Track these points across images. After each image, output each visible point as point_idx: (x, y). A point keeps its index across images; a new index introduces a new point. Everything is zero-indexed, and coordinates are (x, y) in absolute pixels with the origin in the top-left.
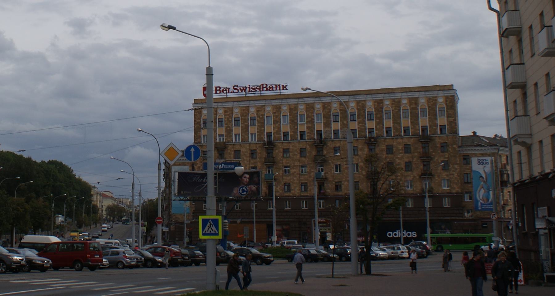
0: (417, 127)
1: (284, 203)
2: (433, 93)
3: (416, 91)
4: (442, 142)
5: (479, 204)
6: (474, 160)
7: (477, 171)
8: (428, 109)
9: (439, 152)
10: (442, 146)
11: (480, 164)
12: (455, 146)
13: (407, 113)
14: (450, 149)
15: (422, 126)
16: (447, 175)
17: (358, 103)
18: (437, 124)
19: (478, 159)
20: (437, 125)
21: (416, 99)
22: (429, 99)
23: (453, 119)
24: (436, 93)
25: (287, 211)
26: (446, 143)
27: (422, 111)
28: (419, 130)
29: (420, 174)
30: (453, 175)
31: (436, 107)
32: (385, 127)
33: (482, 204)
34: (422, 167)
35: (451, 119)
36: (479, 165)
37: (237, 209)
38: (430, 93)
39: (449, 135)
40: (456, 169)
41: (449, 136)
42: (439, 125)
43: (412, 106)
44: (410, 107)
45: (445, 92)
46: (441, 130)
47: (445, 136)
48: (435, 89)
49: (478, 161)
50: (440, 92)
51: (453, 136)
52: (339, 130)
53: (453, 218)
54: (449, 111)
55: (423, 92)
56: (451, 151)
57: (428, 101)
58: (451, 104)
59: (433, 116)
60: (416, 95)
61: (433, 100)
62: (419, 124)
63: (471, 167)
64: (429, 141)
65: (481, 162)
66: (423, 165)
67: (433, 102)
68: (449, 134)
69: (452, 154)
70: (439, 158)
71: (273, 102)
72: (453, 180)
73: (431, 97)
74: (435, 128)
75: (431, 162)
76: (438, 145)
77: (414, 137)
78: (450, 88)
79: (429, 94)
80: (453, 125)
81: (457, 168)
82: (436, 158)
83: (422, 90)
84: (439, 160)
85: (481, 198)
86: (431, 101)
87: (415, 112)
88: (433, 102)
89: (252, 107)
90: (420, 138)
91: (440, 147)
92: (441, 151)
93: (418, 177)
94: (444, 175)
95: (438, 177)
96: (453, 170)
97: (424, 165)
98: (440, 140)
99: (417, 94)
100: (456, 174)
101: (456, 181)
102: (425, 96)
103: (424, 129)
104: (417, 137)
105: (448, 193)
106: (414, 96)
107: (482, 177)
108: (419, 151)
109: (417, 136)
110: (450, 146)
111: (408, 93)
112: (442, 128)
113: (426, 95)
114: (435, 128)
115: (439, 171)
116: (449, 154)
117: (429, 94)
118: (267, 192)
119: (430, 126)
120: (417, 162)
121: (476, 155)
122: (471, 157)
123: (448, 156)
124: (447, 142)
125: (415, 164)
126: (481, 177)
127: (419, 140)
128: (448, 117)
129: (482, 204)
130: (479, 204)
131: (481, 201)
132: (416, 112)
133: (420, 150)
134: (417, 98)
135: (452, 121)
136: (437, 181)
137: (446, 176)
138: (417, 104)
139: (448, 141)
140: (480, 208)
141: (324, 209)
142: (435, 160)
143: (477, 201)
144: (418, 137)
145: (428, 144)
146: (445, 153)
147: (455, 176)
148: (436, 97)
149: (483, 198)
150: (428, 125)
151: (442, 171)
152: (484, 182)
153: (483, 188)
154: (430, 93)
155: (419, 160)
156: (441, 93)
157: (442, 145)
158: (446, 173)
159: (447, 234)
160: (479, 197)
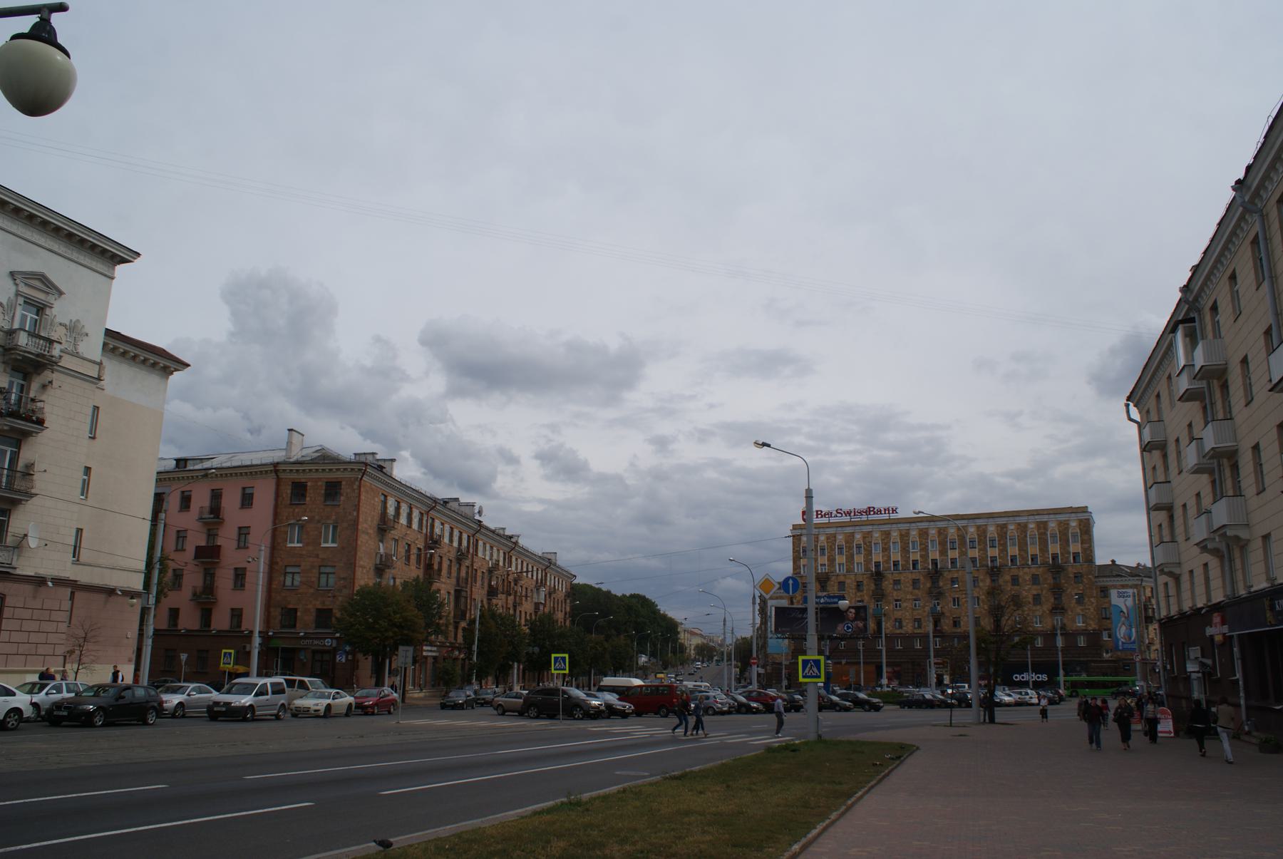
5: (1120, 643)
6: (1114, 593)
10: (1075, 577)
11: (1121, 597)
14: (1085, 580)
16: (1082, 610)
22: (1060, 523)
24: (1068, 515)
28: (1049, 558)
30: (1089, 609)
34: (1052, 600)
35: (1086, 546)
40: (1093, 603)
42: (1071, 552)
45: (1079, 515)
50: (1073, 515)
53: (1089, 659)
60: (1045, 518)
63: (1110, 601)
67: (1064, 526)
70: (1072, 591)
78: (1084, 510)
82: (1069, 590)
85: (1122, 636)
88: (1064, 526)
94: (1079, 609)
95: (1072, 611)
97: (1055, 599)
99: (1047, 517)
101: (1092, 617)
103: (1055, 557)
112: (1076, 556)
115: (1072, 605)
124: (1081, 571)
126: (1122, 611)
128: (1082, 543)
129: (1123, 643)
130: (1120, 643)
131: (1123, 640)
133: (1051, 581)
134: (1046, 522)
136: (1070, 617)
148: (1068, 520)
150: (1059, 552)
151: (1076, 605)
152: (1125, 618)
153: (1124, 624)
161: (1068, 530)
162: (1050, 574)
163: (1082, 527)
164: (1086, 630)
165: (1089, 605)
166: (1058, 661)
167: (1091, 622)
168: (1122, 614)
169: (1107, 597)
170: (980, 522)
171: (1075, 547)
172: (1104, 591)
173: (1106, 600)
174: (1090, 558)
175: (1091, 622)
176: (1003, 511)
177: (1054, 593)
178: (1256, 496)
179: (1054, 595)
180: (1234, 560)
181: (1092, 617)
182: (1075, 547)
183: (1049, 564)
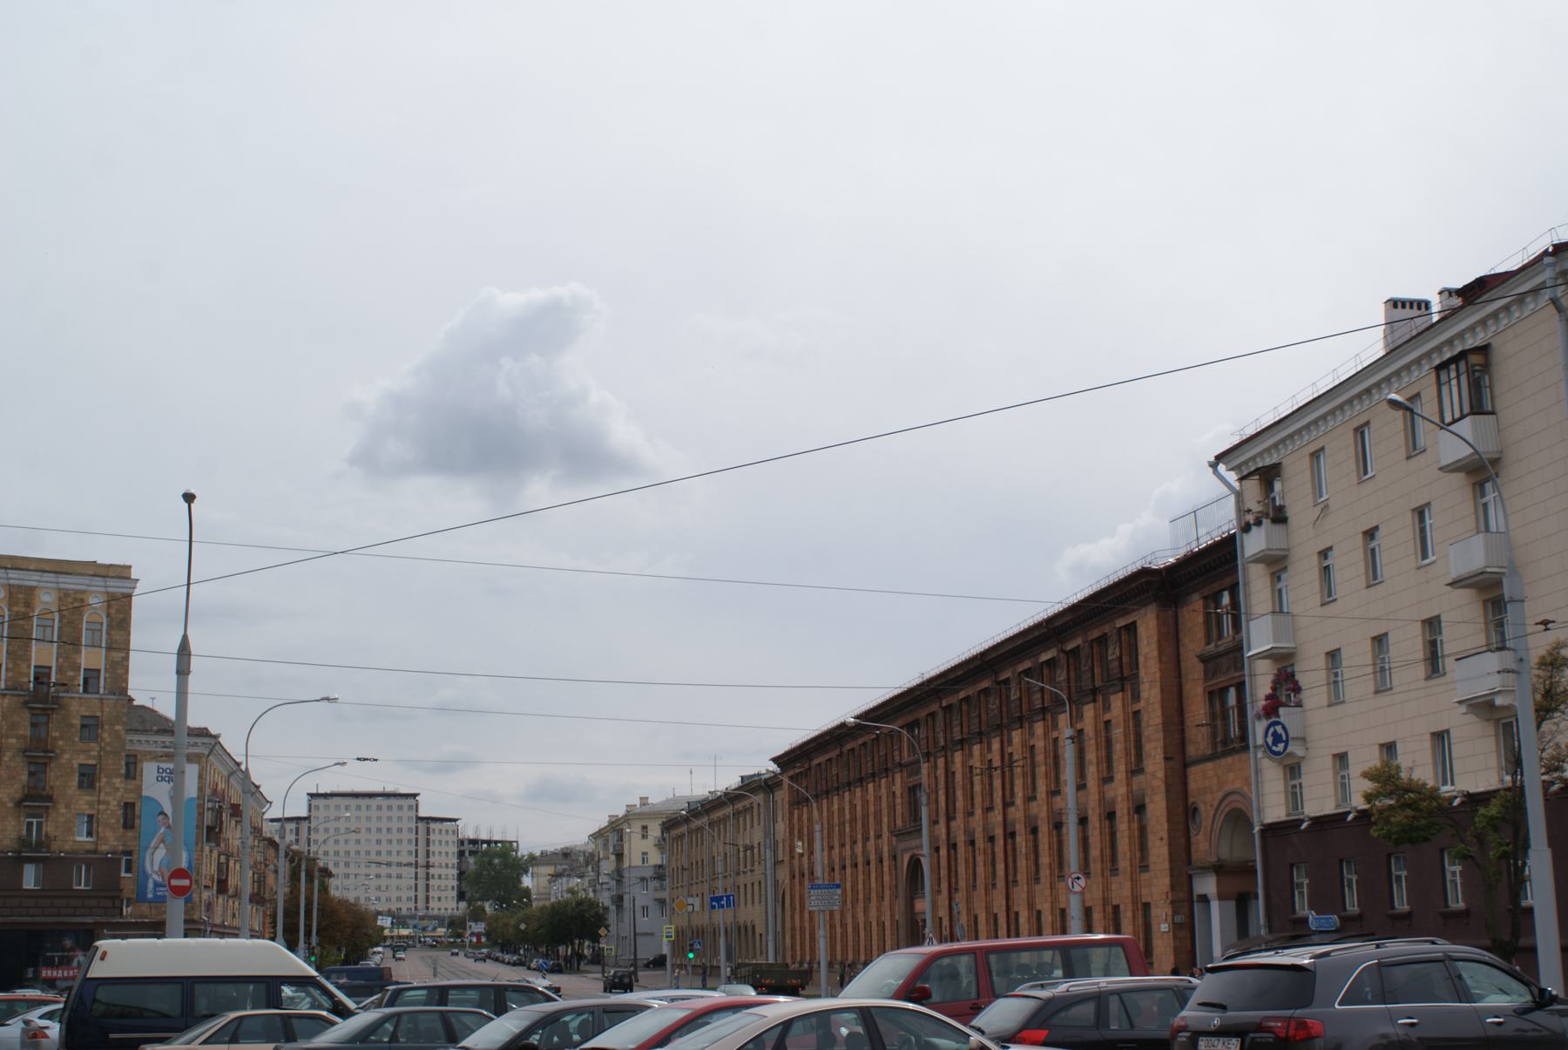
0: (24, 666)
1: (73, 869)
2: (77, 581)
3: (31, 568)
4: (87, 714)
5: (151, 885)
6: (149, 770)
7: (153, 799)
8: (60, 621)
9: (77, 739)
10: (83, 726)
11: (163, 779)
12: (117, 727)
13: (96, 632)
14: (105, 735)
15: (35, 667)
16: (91, 804)
17: (64, 595)
18: (80, 664)
19: (158, 769)
20: (80, 667)
21: (30, 591)
22: (64, 595)
23: (123, 655)
24: (86, 580)
25: (81, 895)
26: (98, 717)
27: (91, 629)
28: (28, 675)
29: (18, 796)
30: (107, 803)
31: (82, 620)
32: (33, 664)
33: (156, 885)
34: (25, 777)
35: (117, 656)
36: (160, 783)
37: (78, 888)
38: (71, 581)
39: (104, 697)
40: (117, 789)
41: (106, 699)
42: (83, 666)
43: (15, 609)
44: (9, 610)
45: (111, 582)
46: (86, 680)
47: (96, 699)
48: (83, 571)
49: (158, 772)
50: (99, 581)
51: (117, 700)
52: (99, 671)
53: (99, 919)
54: (113, 633)
55: (52, 575)
56: (108, 740)
57: (60, 599)
58: (121, 616)
59: (70, 643)
60: (31, 579)
61: (75, 600)
62: (30, 660)
63: (140, 788)
64: (53, 709)
65: (164, 774)
66: (27, 773)
67: (72, 607)
68: (108, 694)
69: (109, 748)
70: (73, 755)
71: (63, 580)
72: (105, 816)
73: (73, 590)
74: (71, 673)
75: (52, 765)
76: (74, 721)
77: (13, 695)
78: (122, 573)
79: (67, 580)
80: (119, 671)
81: (117, 785)
82: (67, 756)
83: (47, 569)
84: (74, 762)
85: (156, 867)
86: (70, 600)
87: (23, 625)
88: (72, 607)
89: (45, 590)
90: (27, 698)
91: (79, 726)
92: (81, 738)
93: (10, 805)
94: (83, 802)
95: (68, 806)
96: (108, 790)
97: (31, 774)
98: (83, 709)
99: (36, 576)
100: (115, 803)
101: (113, 821)
102: (55, 585)
103: (42, 676)
104: (19, 695)
105: (88, 852)
106: (27, 583)
107: (166, 815)
108: (21, 732)
109: (22, 693)
110: (106, 727)
111: (9, 571)
112: (91, 677)
113: (58, 583)
114: (71, 673)
115: (70, 792)
116: (101, 749)
117: (67, 580)
118: (526, 858)
119: (60, 670)
120: (13, 764)
121: (156, 757)
122: (142, 762)
123: (99, 752)
124: (99, 714)
125: (8, 767)
126: (162, 813)
127: (25, 703)
128: (109, 649)
129: (156, 885)
130: (151, 885)
131: (156, 877)
132: (26, 627)
133: (26, 730)
134: (32, 589)
135: (120, 660)
136: (62, 819)
137: (87, 807)
138: (29, 604)
139: (102, 711)
140: (150, 896)
141: (38, 890)
142: (64, 761)
143: (147, 877)
144: (24, 696)
145: (48, 715)
146: (91, 744)
147: (111, 807)
148: (83, 592)
149: (160, 868)
150: (54, 665)
151: (77, 793)
152: (169, 827)
153: (163, 841)
154: (71, 581)
155: (19, 759)
156: (97, 583)
157: (85, 722)
158: (88, 798)
159: (359, 966)
160: (152, 865)
161: (81, 615)
162: (27, 714)
163: (112, 611)
164: (95, 852)
165: (107, 794)
166: (1088, 975)
167: (109, 834)
168: (161, 817)
169: (135, 778)
170: (69, 583)
171: (90, 658)
172: (132, 771)
173: (132, 785)
174: (119, 687)
175: (109, 834)
176: (1016, 630)
177: (31, 761)
178: (1423, 681)
179: (30, 763)
180: (1262, 783)
181: (113, 821)
182: (90, 658)
183: (30, 692)
